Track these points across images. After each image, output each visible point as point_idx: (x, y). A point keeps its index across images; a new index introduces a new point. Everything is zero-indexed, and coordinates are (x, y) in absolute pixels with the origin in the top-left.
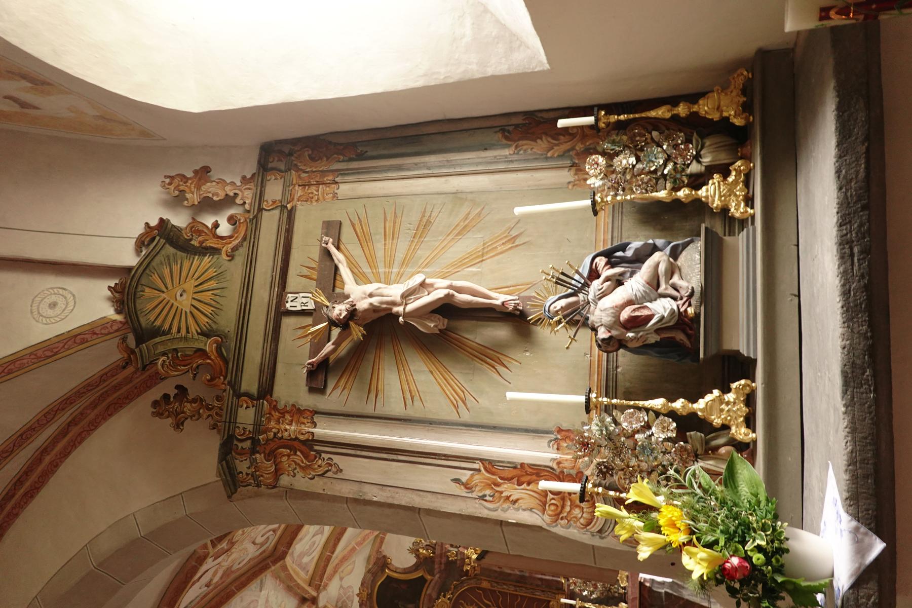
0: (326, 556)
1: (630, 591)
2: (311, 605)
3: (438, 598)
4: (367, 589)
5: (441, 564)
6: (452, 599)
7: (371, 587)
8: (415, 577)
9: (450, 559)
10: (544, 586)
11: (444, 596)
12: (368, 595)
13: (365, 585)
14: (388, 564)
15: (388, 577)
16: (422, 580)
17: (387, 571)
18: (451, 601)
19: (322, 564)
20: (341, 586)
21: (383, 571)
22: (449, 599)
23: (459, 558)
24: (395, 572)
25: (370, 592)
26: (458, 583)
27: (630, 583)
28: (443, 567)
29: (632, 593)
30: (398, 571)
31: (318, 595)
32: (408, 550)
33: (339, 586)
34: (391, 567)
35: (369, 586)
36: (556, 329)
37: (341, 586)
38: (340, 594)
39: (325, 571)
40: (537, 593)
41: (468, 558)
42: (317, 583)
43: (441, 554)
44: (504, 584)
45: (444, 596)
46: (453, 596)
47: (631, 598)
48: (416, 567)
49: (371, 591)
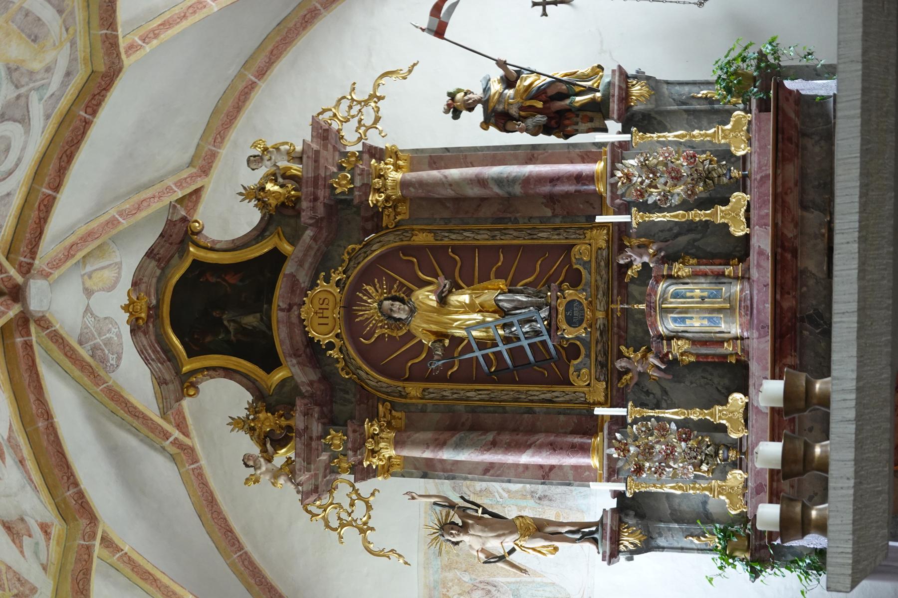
0: (40, 196)
1: (753, 165)
2: (9, 302)
3: (313, 285)
4: (148, 294)
5: (316, 199)
6: (345, 284)
7: (157, 291)
8: (257, 254)
9: (338, 191)
10: (558, 220)
11: (327, 280)
12: (149, 308)
13: (143, 287)
14: (193, 233)
15: (195, 262)
16: (276, 258)
17: (191, 249)
18: (342, 290)
19: (34, 215)
20: (88, 310)
21: (182, 250)
22: (338, 283)
23: (358, 183)
24: (212, 249)
25: (154, 302)
26: (358, 247)
27: (755, 144)
28: (321, 211)
29: (760, 168)
30: (218, 246)
31: (26, 283)
32: (241, 194)
33: (82, 309)
34: (202, 241)
35: (153, 291)
36: (679, 492)
37: (88, 310)
38: (87, 327)
39: (41, 233)
40: (541, 235)
41: (380, 176)
42: (22, 259)
43: (316, 178)
44: (465, 230)
45: (327, 280)
46: (348, 278)
47: (758, 177)
48: (260, 233)
49: (158, 302)
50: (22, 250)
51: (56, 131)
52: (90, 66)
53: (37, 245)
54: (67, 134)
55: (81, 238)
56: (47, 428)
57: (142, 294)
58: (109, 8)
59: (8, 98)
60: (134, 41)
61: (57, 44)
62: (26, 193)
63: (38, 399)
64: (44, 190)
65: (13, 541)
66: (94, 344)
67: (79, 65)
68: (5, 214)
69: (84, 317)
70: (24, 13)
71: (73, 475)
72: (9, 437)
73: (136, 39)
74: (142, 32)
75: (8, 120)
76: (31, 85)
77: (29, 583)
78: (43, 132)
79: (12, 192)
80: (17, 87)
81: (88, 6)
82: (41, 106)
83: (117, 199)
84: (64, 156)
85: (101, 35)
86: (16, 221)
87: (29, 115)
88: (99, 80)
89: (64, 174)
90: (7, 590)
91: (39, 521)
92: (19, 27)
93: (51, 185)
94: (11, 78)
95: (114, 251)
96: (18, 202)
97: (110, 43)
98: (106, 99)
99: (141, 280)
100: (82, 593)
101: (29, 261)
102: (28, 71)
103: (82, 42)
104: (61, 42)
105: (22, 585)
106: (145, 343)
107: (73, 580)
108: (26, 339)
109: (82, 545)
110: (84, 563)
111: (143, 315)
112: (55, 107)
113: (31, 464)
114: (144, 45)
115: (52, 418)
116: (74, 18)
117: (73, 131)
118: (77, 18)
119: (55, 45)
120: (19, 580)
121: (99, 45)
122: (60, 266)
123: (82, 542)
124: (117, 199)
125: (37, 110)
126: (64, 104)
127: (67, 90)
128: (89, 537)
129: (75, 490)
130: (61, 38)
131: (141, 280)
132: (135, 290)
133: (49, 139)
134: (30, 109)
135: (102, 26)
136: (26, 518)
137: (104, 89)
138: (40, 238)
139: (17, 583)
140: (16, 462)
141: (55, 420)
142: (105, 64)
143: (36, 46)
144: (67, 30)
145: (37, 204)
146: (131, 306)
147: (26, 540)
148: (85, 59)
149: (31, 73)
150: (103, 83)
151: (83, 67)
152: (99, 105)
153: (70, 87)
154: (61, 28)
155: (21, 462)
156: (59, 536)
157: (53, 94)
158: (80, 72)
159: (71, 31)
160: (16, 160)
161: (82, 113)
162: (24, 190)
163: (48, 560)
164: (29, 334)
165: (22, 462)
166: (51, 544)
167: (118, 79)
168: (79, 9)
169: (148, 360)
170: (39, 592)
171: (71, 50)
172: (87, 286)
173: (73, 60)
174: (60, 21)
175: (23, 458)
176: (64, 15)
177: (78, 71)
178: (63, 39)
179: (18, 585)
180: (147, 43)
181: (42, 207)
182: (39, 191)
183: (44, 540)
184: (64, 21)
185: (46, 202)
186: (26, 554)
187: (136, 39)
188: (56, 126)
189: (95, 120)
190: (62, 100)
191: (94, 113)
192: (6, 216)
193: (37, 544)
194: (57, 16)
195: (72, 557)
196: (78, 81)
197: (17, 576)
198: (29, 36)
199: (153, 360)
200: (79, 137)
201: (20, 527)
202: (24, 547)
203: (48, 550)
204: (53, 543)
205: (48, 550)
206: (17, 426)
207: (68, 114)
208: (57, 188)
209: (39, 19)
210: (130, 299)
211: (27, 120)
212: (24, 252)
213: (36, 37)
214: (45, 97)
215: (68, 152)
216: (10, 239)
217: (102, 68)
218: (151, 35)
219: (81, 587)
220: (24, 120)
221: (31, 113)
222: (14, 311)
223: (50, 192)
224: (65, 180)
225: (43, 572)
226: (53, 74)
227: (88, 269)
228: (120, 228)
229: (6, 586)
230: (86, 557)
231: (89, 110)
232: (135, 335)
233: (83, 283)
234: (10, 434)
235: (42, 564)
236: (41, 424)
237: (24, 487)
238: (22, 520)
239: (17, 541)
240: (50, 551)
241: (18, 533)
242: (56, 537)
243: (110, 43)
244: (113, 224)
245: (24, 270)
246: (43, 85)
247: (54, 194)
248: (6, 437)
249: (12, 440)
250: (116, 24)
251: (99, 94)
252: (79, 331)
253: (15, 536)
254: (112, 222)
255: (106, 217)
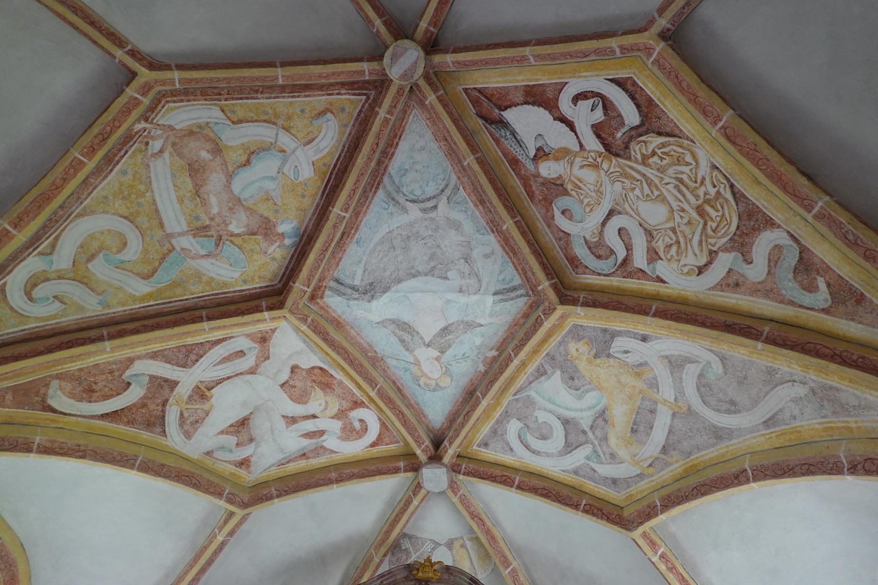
0: (513, 476)
13: (446, 576)
38: (423, 544)
39: (483, 478)
42: (464, 466)
50: (470, 465)
51: (566, 485)
52: (626, 504)
53: (474, 476)
54: (565, 492)
55: (489, 530)
56: (330, 479)
57: (439, 574)
58: (681, 499)
59: (582, 421)
60: (660, 547)
61: (636, 458)
62: (515, 467)
63: (353, 475)
64: (518, 478)
65: (231, 426)
66: (410, 552)
67: (625, 492)
68: (497, 449)
69: (430, 540)
70: (653, 407)
71: (288, 494)
72: (326, 449)
73: (662, 550)
74: (669, 554)
75: (565, 430)
76: (596, 443)
77: (195, 432)
78: (563, 471)
79: (514, 453)
80: (592, 427)
81: (677, 481)
82: (583, 461)
83: (527, 569)
84: (546, 492)
85: (655, 501)
86: (492, 461)
87: (573, 450)
88: (616, 513)
89: (531, 492)
90: (187, 406)
91: (252, 459)
92: (639, 408)
93: (522, 484)
94: (597, 417)
95: (485, 571)
96: (508, 460)
97: (649, 513)
98: (599, 520)
99: (452, 574)
100: (176, 476)
101: (462, 471)
102: (607, 434)
103: (643, 486)
104: (637, 463)
105: (192, 424)
106: (398, 577)
107: (194, 473)
108: (402, 469)
109: (225, 491)
110: (206, 487)
111: (420, 574)
112: (585, 477)
113: (302, 465)
114: (658, 556)
115: (336, 483)
116: (662, 469)
117: (568, 496)
118: (663, 472)
119: (635, 456)
120: (197, 422)
121: (645, 503)
122: (462, 504)
123: (227, 492)
124: (527, 569)
125: (578, 458)
126: (590, 486)
127: (601, 487)
128: (230, 498)
129: (275, 495)
130: (641, 461)
131: (452, 574)
132: (443, 568)
133: (559, 480)
134: (578, 450)
135: (662, 499)
136: (253, 445)
137: (608, 518)
138: (479, 478)
139: (194, 418)
140: (303, 449)
141: (335, 486)
142: (631, 514)
143: (629, 435)
144: (650, 465)
145: (507, 474)
146: (429, 564)
147: (233, 440)
148: (631, 496)
149: (605, 438)
150: (614, 516)
151: (624, 497)
152: (594, 515)
153: (604, 488)
154: (651, 457)
155: (304, 454)
156: (240, 477)
157: (595, 471)
158: (619, 495)
159: (651, 470)
160: (538, 449)
161: (584, 502)
162: (517, 465)
163: (217, 459)
164: (405, 471)
165: (304, 455)
166: (231, 466)
167: (620, 529)
168: (671, 471)
169: (382, 577)
170: (186, 440)
171: (634, 477)
172: (455, 542)
173: (628, 482)
174: (656, 454)
175: (308, 458)
176: (662, 456)
177: (619, 492)
178: (641, 464)
179: (192, 419)
180: (660, 559)
181: (504, 478)
182: (517, 474)
183: (235, 459)
184: (657, 458)
185: (508, 480)
186: (221, 436)
187: (662, 550)
188: (571, 483)
189: (580, 513)
190: (593, 484)
191: (585, 511)
192: (495, 451)
193: (231, 451)
194: (659, 448)
195: (216, 480)
196: (611, 495)
197: (200, 420)
198: (635, 423)
199: (382, 582)
200: (563, 501)
201: (244, 436)
202: (227, 436)
203: (225, 461)
204: (232, 469)
205: (225, 461)
206: (335, 458)
207: (581, 492)
208: (519, 488)
209: (651, 428)
210: (435, 563)
211: (569, 449)
212: (469, 467)
213: (636, 431)
214: (590, 463)
215: (550, 494)
216: (479, 458)
217: (626, 514)
218: (670, 566)
219: (183, 478)
220: (569, 447)
221: (575, 451)
222: (423, 458)
223: (516, 483)
224: (527, 494)
225: (205, 451)
226: (610, 463)
227: (469, 544)
228: (501, 568)
229: (190, 406)
230: (212, 491)
231: (588, 507)
232: (405, 568)
233: (456, 539)
234: (328, 449)
235: (212, 452)
236: (334, 475)
237: (282, 451)
238: (251, 440)
239: (232, 429)
240: (225, 464)
241: (239, 432)
242: (238, 473)
243: (649, 513)
244: (504, 562)
245: (455, 468)
246: (599, 456)
247: (515, 486)
248: (324, 444)
249: (322, 451)
250: (667, 510)
251: (603, 514)
252: (419, 535)
253: (236, 428)
254: (506, 563)
255: (510, 557)
